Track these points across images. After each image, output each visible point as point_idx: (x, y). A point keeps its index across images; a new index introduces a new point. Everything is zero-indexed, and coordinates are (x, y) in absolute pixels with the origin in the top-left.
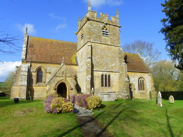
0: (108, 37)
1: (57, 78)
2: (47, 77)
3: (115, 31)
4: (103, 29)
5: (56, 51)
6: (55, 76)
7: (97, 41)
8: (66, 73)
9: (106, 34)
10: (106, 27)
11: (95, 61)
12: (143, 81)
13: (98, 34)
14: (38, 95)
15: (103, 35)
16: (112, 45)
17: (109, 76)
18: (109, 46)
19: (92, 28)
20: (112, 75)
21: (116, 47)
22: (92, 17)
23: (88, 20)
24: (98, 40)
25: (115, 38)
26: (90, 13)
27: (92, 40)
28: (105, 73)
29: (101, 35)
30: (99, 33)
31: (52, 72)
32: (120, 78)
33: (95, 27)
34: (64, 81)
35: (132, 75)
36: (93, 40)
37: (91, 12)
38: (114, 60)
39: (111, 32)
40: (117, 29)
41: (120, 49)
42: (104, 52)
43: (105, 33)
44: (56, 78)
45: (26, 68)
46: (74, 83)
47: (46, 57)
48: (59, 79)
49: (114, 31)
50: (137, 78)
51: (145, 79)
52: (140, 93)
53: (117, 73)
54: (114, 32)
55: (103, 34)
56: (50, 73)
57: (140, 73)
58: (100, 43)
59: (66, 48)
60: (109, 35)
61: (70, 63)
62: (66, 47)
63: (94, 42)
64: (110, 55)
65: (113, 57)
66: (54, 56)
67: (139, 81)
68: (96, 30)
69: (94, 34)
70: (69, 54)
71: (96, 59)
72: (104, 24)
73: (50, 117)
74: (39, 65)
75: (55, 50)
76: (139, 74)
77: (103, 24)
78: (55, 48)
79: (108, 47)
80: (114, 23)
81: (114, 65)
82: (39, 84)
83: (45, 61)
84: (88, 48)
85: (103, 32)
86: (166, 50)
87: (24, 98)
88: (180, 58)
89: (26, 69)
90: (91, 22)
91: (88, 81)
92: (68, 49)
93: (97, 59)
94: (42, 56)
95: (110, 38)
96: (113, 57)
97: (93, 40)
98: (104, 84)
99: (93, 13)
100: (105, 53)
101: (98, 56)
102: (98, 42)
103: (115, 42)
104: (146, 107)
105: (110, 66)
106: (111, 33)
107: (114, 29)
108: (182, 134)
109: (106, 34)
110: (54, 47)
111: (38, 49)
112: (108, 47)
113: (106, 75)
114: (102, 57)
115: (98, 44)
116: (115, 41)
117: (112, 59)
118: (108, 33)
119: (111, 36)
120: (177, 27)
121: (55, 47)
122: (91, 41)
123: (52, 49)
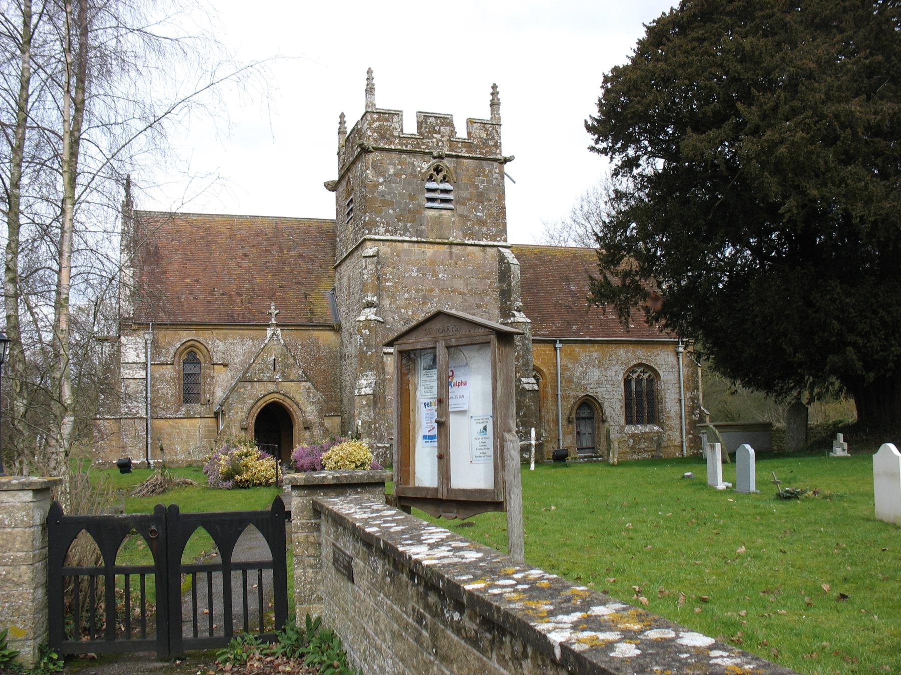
0: (449, 212)
1: (252, 387)
2: (220, 383)
3: (483, 182)
4: (431, 179)
5: (248, 270)
6: (245, 380)
7: (404, 234)
8: (286, 366)
10: (441, 171)
11: (396, 317)
12: (650, 381)
13: (407, 204)
14: (189, 453)
15: (430, 204)
16: (471, 242)
18: (455, 249)
19: (381, 180)
21: (488, 249)
22: (382, 137)
24: (406, 230)
25: (482, 211)
26: (372, 118)
27: (382, 230)
29: (420, 206)
30: (412, 197)
31: (237, 360)
33: (395, 174)
34: (276, 397)
35: (595, 355)
36: (387, 231)
37: (376, 116)
38: (479, 306)
39: (467, 189)
40: (490, 171)
42: (435, 274)
44: (249, 386)
45: (139, 351)
46: (320, 403)
47: (209, 302)
48: (259, 390)
49: (477, 181)
50: (617, 368)
51: (657, 374)
52: (633, 436)
54: (477, 187)
55: (430, 200)
56: (226, 365)
57: (631, 348)
58: (414, 239)
59: (293, 253)
60: (457, 202)
61: (303, 321)
62: (289, 249)
63: (389, 237)
64: (459, 284)
65: (473, 293)
66: (240, 295)
67: (627, 382)
68: (398, 188)
69: (390, 204)
70: (304, 281)
71: (398, 308)
72: (435, 158)
74: (186, 336)
75: (245, 263)
76: (627, 352)
77: (426, 158)
78: (245, 255)
79: (451, 253)
80: (477, 146)
82: (188, 410)
83: (207, 319)
84: (366, 268)
85: (429, 190)
87: (138, 462)
89: (138, 356)
90: (377, 156)
91: (365, 395)
92: (300, 256)
93: (406, 308)
94: (195, 298)
95: (461, 216)
96: (473, 293)
97: (387, 231)
99: (387, 120)
100: (438, 279)
101: (406, 295)
102: (407, 239)
103: (484, 229)
106: (465, 194)
107: (479, 172)
108: (78, 468)
110: (240, 252)
111: (176, 266)
112: (451, 253)
114: (424, 297)
115: (406, 245)
116: (482, 223)
117: (472, 300)
118: (450, 196)
119: (464, 204)
120: (74, 542)
121: (247, 250)
122: (377, 237)
123: (232, 264)
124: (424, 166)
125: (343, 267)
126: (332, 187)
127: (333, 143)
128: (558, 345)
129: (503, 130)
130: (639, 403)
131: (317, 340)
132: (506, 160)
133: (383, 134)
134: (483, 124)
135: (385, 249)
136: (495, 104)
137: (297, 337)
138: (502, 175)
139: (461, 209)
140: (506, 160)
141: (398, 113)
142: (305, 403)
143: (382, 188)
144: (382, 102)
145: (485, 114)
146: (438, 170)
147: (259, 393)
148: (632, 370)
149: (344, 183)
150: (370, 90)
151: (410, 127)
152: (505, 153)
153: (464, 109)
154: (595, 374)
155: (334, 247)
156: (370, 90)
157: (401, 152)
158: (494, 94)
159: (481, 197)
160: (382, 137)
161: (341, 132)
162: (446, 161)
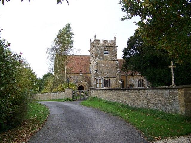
2: (73, 82)
4: (105, 50)
9: (107, 54)
12: (142, 82)
17: (109, 80)
20: (111, 80)
22: (97, 44)
23: (94, 46)
28: (106, 79)
32: (116, 81)
34: (81, 85)
41: (116, 62)
43: (106, 53)
53: (115, 78)
64: (110, 67)
67: (138, 82)
68: (100, 52)
69: (99, 54)
73: (57, 106)
81: (112, 73)
86: (75, 94)
88: (147, 16)
90: (96, 47)
98: (106, 85)
104: (128, 107)
105: (110, 74)
106: (110, 52)
109: (107, 54)
113: (107, 80)
124: (104, 48)
125: (91, 64)
126: (89, 51)
127: (89, 44)
128: (127, 76)
129: (116, 42)
130: (107, 83)
131: (87, 76)
132: (117, 47)
133: (97, 43)
134: (113, 41)
135: (98, 61)
136: (115, 38)
137: (84, 75)
138: (116, 49)
139: (110, 55)
140: (117, 47)
141: (100, 40)
142: (86, 85)
143: (97, 52)
144: (97, 38)
145: (113, 39)
146: (106, 49)
147: (78, 84)
148: (139, 80)
149: (91, 50)
150: (95, 37)
151: (101, 42)
152: (117, 46)
153: (111, 38)
154: (133, 81)
155: (90, 60)
156: (95, 37)
157: (100, 46)
158: (115, 36)
159: (113, 53)
160: (97, 44)
161: (91, 42)
162: (107, 48)
